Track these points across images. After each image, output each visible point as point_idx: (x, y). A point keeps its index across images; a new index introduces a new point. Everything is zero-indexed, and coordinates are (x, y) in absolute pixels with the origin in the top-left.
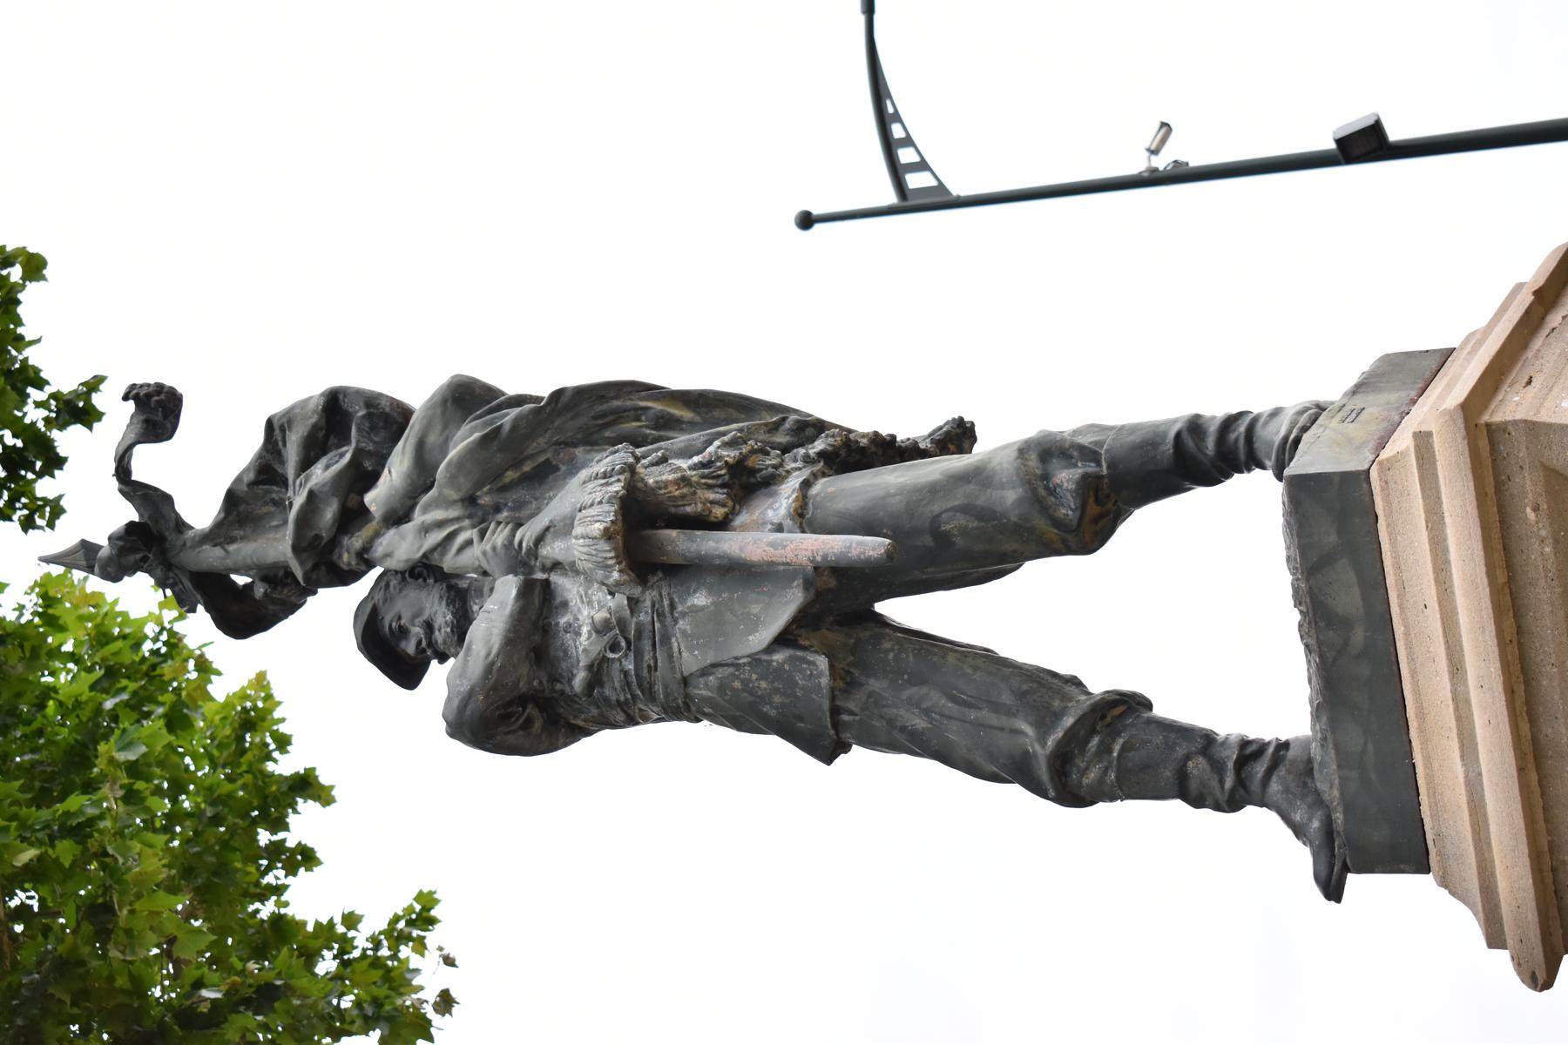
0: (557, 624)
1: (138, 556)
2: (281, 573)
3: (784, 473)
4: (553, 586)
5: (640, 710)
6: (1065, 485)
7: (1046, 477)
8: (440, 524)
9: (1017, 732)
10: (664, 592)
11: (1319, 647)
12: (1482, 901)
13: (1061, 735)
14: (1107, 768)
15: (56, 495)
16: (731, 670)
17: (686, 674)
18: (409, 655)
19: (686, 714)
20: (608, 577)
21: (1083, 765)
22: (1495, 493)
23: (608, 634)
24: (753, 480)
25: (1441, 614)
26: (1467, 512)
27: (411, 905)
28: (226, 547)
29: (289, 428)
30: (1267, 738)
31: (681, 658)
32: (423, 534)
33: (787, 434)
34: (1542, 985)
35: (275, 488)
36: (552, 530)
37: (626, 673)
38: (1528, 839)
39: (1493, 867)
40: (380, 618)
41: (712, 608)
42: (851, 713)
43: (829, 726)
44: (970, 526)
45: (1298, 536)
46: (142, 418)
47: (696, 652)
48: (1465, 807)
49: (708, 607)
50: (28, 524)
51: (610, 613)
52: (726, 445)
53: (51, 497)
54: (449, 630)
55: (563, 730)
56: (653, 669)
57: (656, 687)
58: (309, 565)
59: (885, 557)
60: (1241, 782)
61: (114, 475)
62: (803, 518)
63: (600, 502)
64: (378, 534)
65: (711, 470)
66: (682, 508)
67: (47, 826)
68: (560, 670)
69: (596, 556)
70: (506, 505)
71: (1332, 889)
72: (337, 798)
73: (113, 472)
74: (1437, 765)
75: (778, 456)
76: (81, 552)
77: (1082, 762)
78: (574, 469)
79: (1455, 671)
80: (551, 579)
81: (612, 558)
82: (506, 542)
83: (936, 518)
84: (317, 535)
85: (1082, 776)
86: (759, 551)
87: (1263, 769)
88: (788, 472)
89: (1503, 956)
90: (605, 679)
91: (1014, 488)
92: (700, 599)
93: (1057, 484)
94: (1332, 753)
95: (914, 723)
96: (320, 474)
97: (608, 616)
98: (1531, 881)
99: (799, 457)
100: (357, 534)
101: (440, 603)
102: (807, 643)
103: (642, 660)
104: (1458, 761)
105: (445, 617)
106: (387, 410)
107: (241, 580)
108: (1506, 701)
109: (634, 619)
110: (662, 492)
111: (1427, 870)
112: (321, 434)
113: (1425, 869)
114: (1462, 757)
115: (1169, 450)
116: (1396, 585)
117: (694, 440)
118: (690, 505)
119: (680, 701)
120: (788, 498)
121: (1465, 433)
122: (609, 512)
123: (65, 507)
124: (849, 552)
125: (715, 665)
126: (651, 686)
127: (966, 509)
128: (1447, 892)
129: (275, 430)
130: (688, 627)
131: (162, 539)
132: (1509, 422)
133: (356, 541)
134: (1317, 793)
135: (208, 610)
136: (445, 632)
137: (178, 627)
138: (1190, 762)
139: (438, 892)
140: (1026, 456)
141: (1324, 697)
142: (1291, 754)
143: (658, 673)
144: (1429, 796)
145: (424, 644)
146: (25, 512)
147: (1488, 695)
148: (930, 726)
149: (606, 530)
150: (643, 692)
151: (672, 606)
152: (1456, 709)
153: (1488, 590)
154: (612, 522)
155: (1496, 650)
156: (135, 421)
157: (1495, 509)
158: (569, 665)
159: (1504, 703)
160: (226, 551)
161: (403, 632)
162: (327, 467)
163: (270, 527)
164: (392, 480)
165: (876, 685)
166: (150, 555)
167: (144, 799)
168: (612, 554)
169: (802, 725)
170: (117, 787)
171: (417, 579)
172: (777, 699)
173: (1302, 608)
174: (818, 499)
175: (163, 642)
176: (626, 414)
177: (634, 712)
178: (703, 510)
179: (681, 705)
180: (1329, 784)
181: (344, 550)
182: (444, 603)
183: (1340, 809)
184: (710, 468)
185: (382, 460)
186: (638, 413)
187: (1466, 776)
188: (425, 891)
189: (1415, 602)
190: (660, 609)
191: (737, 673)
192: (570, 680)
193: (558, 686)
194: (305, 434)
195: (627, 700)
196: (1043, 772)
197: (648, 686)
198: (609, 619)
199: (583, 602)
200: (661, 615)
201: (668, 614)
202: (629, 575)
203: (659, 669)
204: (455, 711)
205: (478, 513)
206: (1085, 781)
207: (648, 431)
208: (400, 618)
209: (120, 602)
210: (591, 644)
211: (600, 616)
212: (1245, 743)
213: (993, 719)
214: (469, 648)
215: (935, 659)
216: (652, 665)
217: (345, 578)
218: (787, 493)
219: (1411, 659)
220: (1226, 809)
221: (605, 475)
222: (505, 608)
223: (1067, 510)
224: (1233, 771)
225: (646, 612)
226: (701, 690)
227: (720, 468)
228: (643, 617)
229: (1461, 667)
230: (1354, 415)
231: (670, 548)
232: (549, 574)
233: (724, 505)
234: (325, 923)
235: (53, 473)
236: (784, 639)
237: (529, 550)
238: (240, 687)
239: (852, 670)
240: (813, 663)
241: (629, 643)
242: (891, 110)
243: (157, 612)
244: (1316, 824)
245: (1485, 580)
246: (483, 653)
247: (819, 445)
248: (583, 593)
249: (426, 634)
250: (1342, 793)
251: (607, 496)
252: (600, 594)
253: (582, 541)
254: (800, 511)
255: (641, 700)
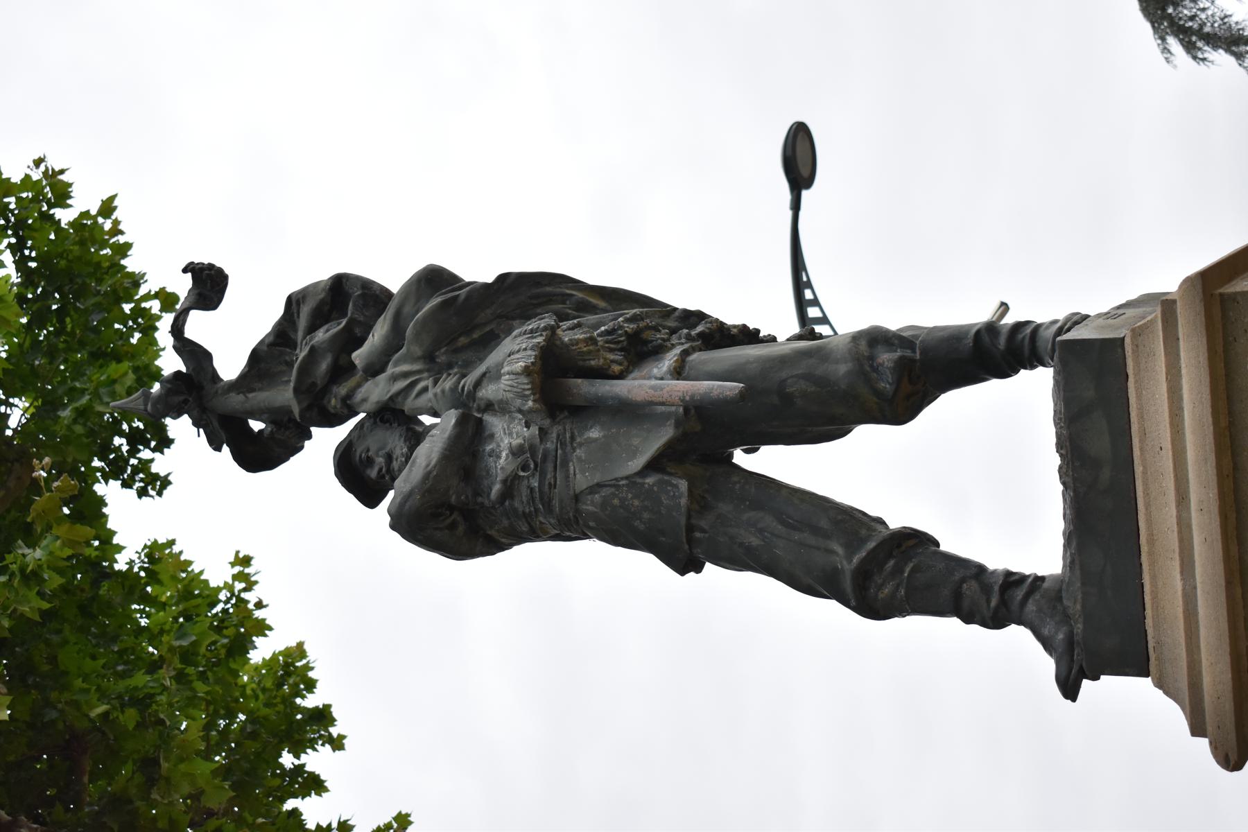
0: (484, 450)
1: (182, 398)
2: (286, 419)
3: (670, 345)
4: (484, 423)
5: (541, 523)
6: (886, 363)
7: (872, 358)
8: (405, 375)
9: (833, 552)
10: (568, 427)
11: (1074, 483)
12: (1189, 696)
13: (864, 554)
14: (898, 585)
15: (166, 473)
16: (613, 490)
17: (577, 491)
18: (372, 479)
19: (575, 526)
20: (524, 405)
21: (880, 581)
22: (1224, 351)
23: (521, 457)
24: (645, 349)
25: (1173, 452)
26: (1200, 362)
27: (391, 822)
28: (248, 395)
29: (303, 302)
30: (1027, 573)
31: (575, 478)
32: (392, 382)
33: (676, 321)
34: (1233, 765)
35: (288, 350)
36: (488, 375)
37: (532, 490)
38: (1230, 639)
39: (1200, 666)
40: (354, 449)
41: (603, 440)
42: (703, 531)
43: (685, 540)
44: (809, 390)
45: (1064, 391)
46: (197, 292)
47: (587, 474)
48: (1181, 616)
49: (600, 439)
50: (142, 493)
51: (524, 440)
52: (627, 320)
53: (162, 474)
54: (403, 459)
55: (481, 540)
56: (553, 486)
57: (554, 502)
58: (305, 404)
59: (739, 396)
60: (1004, 602)
61: (169, 332)
62: (678, 372)
63: (525, 349)
64: (359, 385)
65: (614, 337)
66: (588, 362)
67: (120, 697)
68: (482, 486)
69: (517, 387)
70: (457, 363)
71: (1070, 690)
72: (346, 747)
73: (170, 330)
74: (1161, 583)
75: (667, 334)
76: (141, 399)
77: (880, 579)
78: (509, 332)
79: (1181, 500)
80: (484, 418)
81: (528, 389)
82: (453, 387)
83: (783, 382)
84: (313, 382)
85: (879, 590)
86: (643, 392)
87: (1022, 593)
88: (673, 345)
89: (1204, 743)
90: (515, 493)
91: (846, 363)
92: (595, 433)
93: (880, 363)
94: (1078, 572)
95: (751, 540)
96: (321, 335)
97: (523, 442)
98: (1230, 676)
99: (683, 336)
100: (343, 385)
101: (399, 439)
102: (673, 471)
103: (545, 478)
104: (1178, 577)
105: (402, 449)
106: (378, 292)
107: (256, 425)
108: (1221, 522)
109: (543, 446)
110: (574, 348)
111: (1147, 675)
112: (326, 308)
113: (1145, 674)
114: (1182, 573)
115: (969, 343)
116: (1139, 432)
117: (604, 318)
118: (594, 359)
119: (571, 514)
120: (670, 360)
121: (1202, 296)
122: (530, 356)
123: (172, 480)
124: (711, 393)
125: (599, 486)
126: (550, 500)
127: (807, 377)
128: (1161, 692)
129: (293, 303)
130: (583, 455)
131: (200, 388)
132: (1239, 292)
133: (342, 390)
134: (1065, 609)
135: (227, 445)
136: (401, 461)
137: (243, 595)
138: (965, 585)
139: (412, 815)
140: (858, 342)
141: (1074, 526)
142: (1046, 585)
143: (556, 490)
144: (1152, 609)
145: (384, 470)
146: (142, 484)
147: (1206, 517)
148: (763, 543)
149: (526, 367)
150: (543, 506)
151: (573, 438)
152: (1180, 532)
153: (1212, 428)
154: (532, 363)
155: (1215, 478)
156: (191, 294)
157: (1223, 365)
158: (490, 483)
159: (1218, 523)
160: (246, 397)
161: (370, 462)
162: (328, 331)
163: (283, 382)
164: (373, 341)
165: (725, 508)
166: (190, 399)
167: (191, 682)
168: (529, 386)
169: (664, 539)
170: (171, 668)
171: (385, 423)
172: (646, 515)
173: (1062, 452)
174: (693, 363)
175: (232, 605)
176: (555, 298)
177: (536, 524)
178: (603, 364)
179: (572, 518)
180: (1074, 605)
181: (333, 396)
182: (403, 439)
183: (1081, 620)
184: (613, 335)
185: (368, 328)
186: (565, 298)
187: (1184, 590)
188: (403, 813)
189: (1153, 446)
190: (563, 440)
191: (617, 493)
192: (489, 494)
193: (480, 499)
194: (314, 306)
195: (530, 512)
196: (848, 585)
197: (547, 500)
198: (523, 445)
199: (505, 434)
200: (563, 444)
201: (569, 444)
202: (541, 407)
203: (557, 487)
204: (397, 505)
205: (433, 364)
206: (881, 596)
207: (570, 311)
208: (368, 450)
209: (205, 572)
210: (507, 464)
211: (517, 442)
212: (1009, 574)
213: (811, 540)
214: (414, 462)
215: (771, 491)
216: (553, 483)
217: (332, 421)
218: (669, 361)
219: (1147, 494)
220: (991, 624)
221: (532, 331)
222: (445, 433)
223: (886, 385)
224: (998, 593)
225: (552, 442)
226: (589, 506)
227: (621, 336)
228: (549, 445)
229: (1186, 497)
230: (1117, 316)
231: (575, 391)
232: (483, 414)
233: (620, 364)
234: (325, 826)
235: (163, 450)
236: (654, 465)
237: (469, 392)
238: (285, 647)
239: (706, 496)
240: (676, 486)
241: (536, 465)
242: (805, 279)
243: (231, 582)
244: (1061, 636)
245: (1210, 419)
246: (424, 464)
247: (700, 329)
248: (506, 427)
249: (386, 462)
250: (1083, 606)
251: (530, 345)
252: (519, 427)
253: (507, 376)
254: (678, 370)
255: (541, 513)
